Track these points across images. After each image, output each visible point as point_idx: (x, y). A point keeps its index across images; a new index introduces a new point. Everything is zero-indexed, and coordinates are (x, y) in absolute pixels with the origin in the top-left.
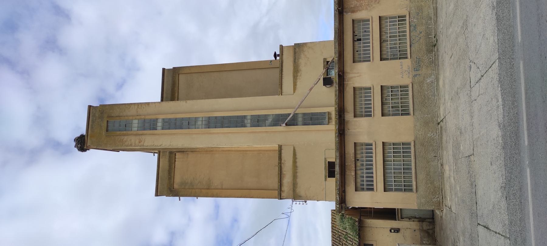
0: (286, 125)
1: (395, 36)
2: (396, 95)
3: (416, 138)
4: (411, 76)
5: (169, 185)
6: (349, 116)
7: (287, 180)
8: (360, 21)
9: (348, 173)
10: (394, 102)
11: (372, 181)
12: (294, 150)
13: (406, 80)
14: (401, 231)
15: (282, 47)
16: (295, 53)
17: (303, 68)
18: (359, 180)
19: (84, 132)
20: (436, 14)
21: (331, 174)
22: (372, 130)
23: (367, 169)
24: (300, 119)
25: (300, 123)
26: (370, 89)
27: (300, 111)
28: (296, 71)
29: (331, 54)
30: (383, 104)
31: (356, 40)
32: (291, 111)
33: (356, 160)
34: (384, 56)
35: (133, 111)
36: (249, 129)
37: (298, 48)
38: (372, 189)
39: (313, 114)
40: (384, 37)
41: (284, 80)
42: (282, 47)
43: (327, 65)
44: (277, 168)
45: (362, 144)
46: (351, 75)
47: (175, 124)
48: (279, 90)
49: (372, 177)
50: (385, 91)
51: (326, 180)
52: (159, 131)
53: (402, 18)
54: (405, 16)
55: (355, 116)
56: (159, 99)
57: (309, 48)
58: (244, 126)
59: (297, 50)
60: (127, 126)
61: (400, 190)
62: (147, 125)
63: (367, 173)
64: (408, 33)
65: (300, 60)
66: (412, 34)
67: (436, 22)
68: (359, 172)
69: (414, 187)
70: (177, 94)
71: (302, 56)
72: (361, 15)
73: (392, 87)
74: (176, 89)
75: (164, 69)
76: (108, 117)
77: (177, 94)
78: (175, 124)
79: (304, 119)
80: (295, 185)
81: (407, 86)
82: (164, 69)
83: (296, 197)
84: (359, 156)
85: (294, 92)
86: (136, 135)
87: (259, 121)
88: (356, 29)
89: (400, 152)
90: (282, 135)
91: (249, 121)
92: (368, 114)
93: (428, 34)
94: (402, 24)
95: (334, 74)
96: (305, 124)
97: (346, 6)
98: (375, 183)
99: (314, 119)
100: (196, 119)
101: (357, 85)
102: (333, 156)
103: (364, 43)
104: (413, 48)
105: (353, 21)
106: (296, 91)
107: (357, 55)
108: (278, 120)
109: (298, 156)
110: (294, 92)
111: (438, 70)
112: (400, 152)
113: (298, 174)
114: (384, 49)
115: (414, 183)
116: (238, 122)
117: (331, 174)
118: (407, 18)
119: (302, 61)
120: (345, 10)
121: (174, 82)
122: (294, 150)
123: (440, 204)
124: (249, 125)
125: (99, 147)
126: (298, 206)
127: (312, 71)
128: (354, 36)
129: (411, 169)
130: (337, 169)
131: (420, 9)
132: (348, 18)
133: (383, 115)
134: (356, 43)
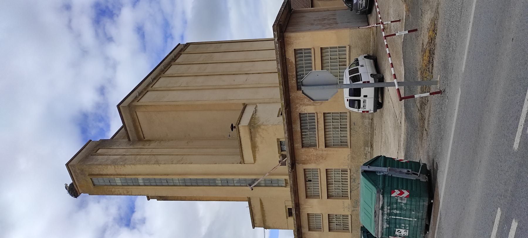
12: (260, 200)
13: (347, 212)
21: (290, 214)
28: (254, 147)
34: (324, 51)
36: (219, 177)
41: (242, 142)
43: (280, 144)
51: (287, 218)
53: (344, 171)
55: (309, 230)
57: (263, 129)
64: (349, 183)
65: (256, 139)
66: (352, 184)
70: (140, 129)
71: (258, 135)
72: (310, 166)
74: (138, 124)
77: (140, 129)
85: (255, 162)
92: (317, 196)
97: (297, 158)
102: (290, 205)
104: (352, 194)
105: (304, 169)
106: (257, 162)
109: (264, 204)
110: (255, 160)
120: (296, 162)
122: (260, 200)
130: (294, 212)
132: (300, 168)
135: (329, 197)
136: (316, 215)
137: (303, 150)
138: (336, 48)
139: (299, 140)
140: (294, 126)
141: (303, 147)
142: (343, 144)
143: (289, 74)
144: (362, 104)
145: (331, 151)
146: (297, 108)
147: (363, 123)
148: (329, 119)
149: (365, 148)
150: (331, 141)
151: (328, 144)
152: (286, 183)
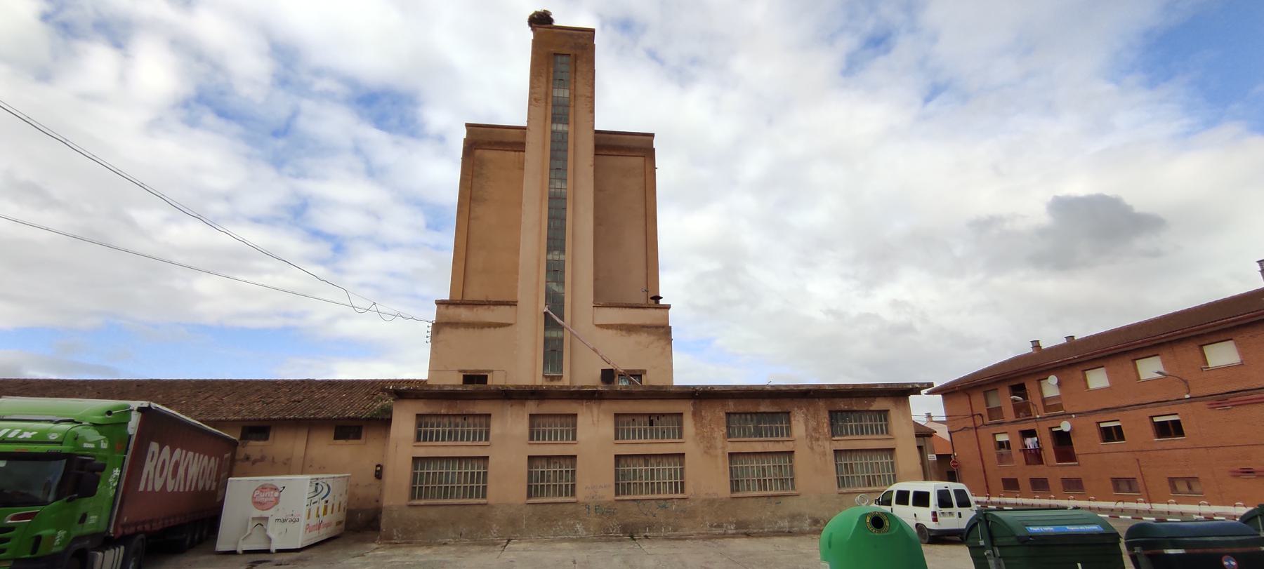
0: (546, 313)
1: (652, 478)
2: (561, 478)
3: (492, 507)
4: (587, 500)
5: (484, 143)
6: (532, 407)
7: (464, 314)
8: (681, 424)
9: (445, 403)
10: (550, 474)
11: (431, 440)
13: (581, 495)
14: (378, 482)
15: (667, 307)
16: (657, 327)
17: (635, 338)
18: (434, 420)
19: (556, 23)
20: (680, 539)
21: (469, 379)
22: (509, 439)
23: (450, 432)
24: (554, 334)
25: (549, 334)
26: (574, 438)
27: (567, 336)
28: (629, 329)
29: (652, 379)
30: (549, 458)
31: (652, 419)
32: (566, 323)
33: (465, 416)
34: (623, 461)
35: (582, 89)
36: (567, 257)
37: (663, 332)
38: (418, 440)
39: (561, 353)
40: (653, 460)
41: (616, 310)
42: (667, 307)
43: (638, 375)
44: (483, 298)
45: (488, 426)
46: (595, 410)
47: (559, 150)
48: (602, 300)
49: (437, 440)
50: (568, 462)
52: (550, 127)
54: (682, 491)
56: (597, 128)
58: (549, 250)
59: (662, 330)
60: (558, 81)
61: (414, 481)
62: (560, 110)
63: (444, 432)
64: (656, 496)
67: (667, 538)
68: (446, 420)
69: (416, 502)
71: (652, 338)
72: (689, 425)
73: (574, 472)
75: (652, 135)
76: (576, 57)
78: (559, 150)
79: (554, 339)
80: (455, 325)
81: (573, 494)
82: (652, 135)
83: (438, 327)
84: (471, 420)
86: (547, 94)
87: (555, 271)
88: (669, 418)
89: (472, 481)
90: (532, 304)
91: (556, 258)
92: (419, 437)
93: (651, 526)
94: (671, 488)
95: (622, 384)
96: (546, 341)
98: (428, 443)
99: (553, 354)
100: (564, 180)
101: (580, 420)
102: (495, 381)
103: (645, 431)
104: (631, 504)
105: (681, 414)
106: (599, 329)
107: (626, 419)
108: (555, 301)
109: (502, 330)
111: (598, 539)
112: (472, 481)
113: (471, 330)
114: (635, 461)
115: (422, 502)
116: (556, 240)
117: (469, 379)
118: (679, 495)
119: (643, 338)
121: (631, 152)
123: (389, 541)
124: (550, 257)
125: (536, 43)
126: (425, 329)
127: (624, 353)
128: (659, 416)
129: (445, 497)
131: (691, 515)
132: (686, 408)
133: (618, 458)
134: (647, 419)
135: (618, 458)
136: (789, 429)
137: (722, 414)
138: (682, 477)
139: (741, 408)
140: (768, 401)
141: (728, 414)
142: (735, 485)
143: (854, 401)
144: (944, 510)
145: (723, 465)
146: (800, 408)
147: (782, 518)
148: (783, 462)
149: (731, 523)
150: (742, 464)
151: (735, 457)
152: (552, 378)
